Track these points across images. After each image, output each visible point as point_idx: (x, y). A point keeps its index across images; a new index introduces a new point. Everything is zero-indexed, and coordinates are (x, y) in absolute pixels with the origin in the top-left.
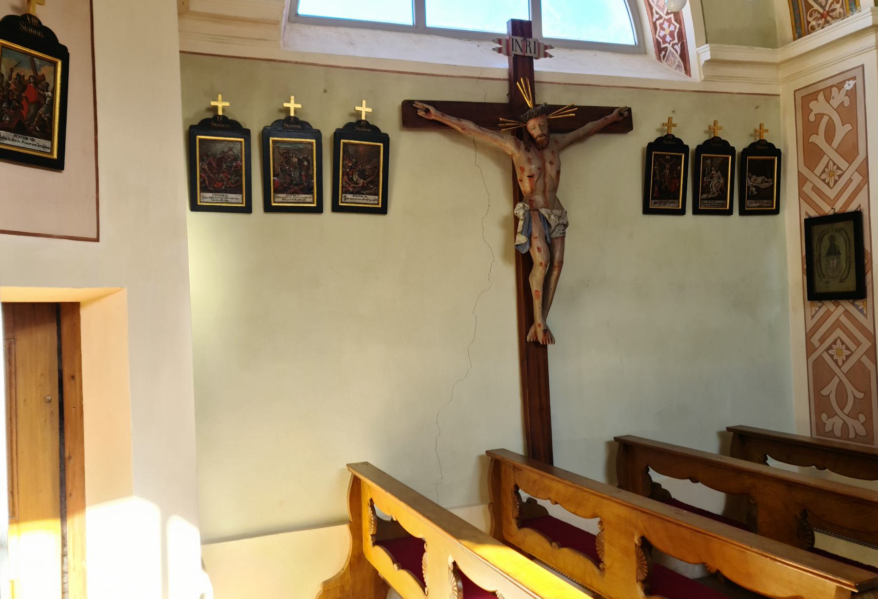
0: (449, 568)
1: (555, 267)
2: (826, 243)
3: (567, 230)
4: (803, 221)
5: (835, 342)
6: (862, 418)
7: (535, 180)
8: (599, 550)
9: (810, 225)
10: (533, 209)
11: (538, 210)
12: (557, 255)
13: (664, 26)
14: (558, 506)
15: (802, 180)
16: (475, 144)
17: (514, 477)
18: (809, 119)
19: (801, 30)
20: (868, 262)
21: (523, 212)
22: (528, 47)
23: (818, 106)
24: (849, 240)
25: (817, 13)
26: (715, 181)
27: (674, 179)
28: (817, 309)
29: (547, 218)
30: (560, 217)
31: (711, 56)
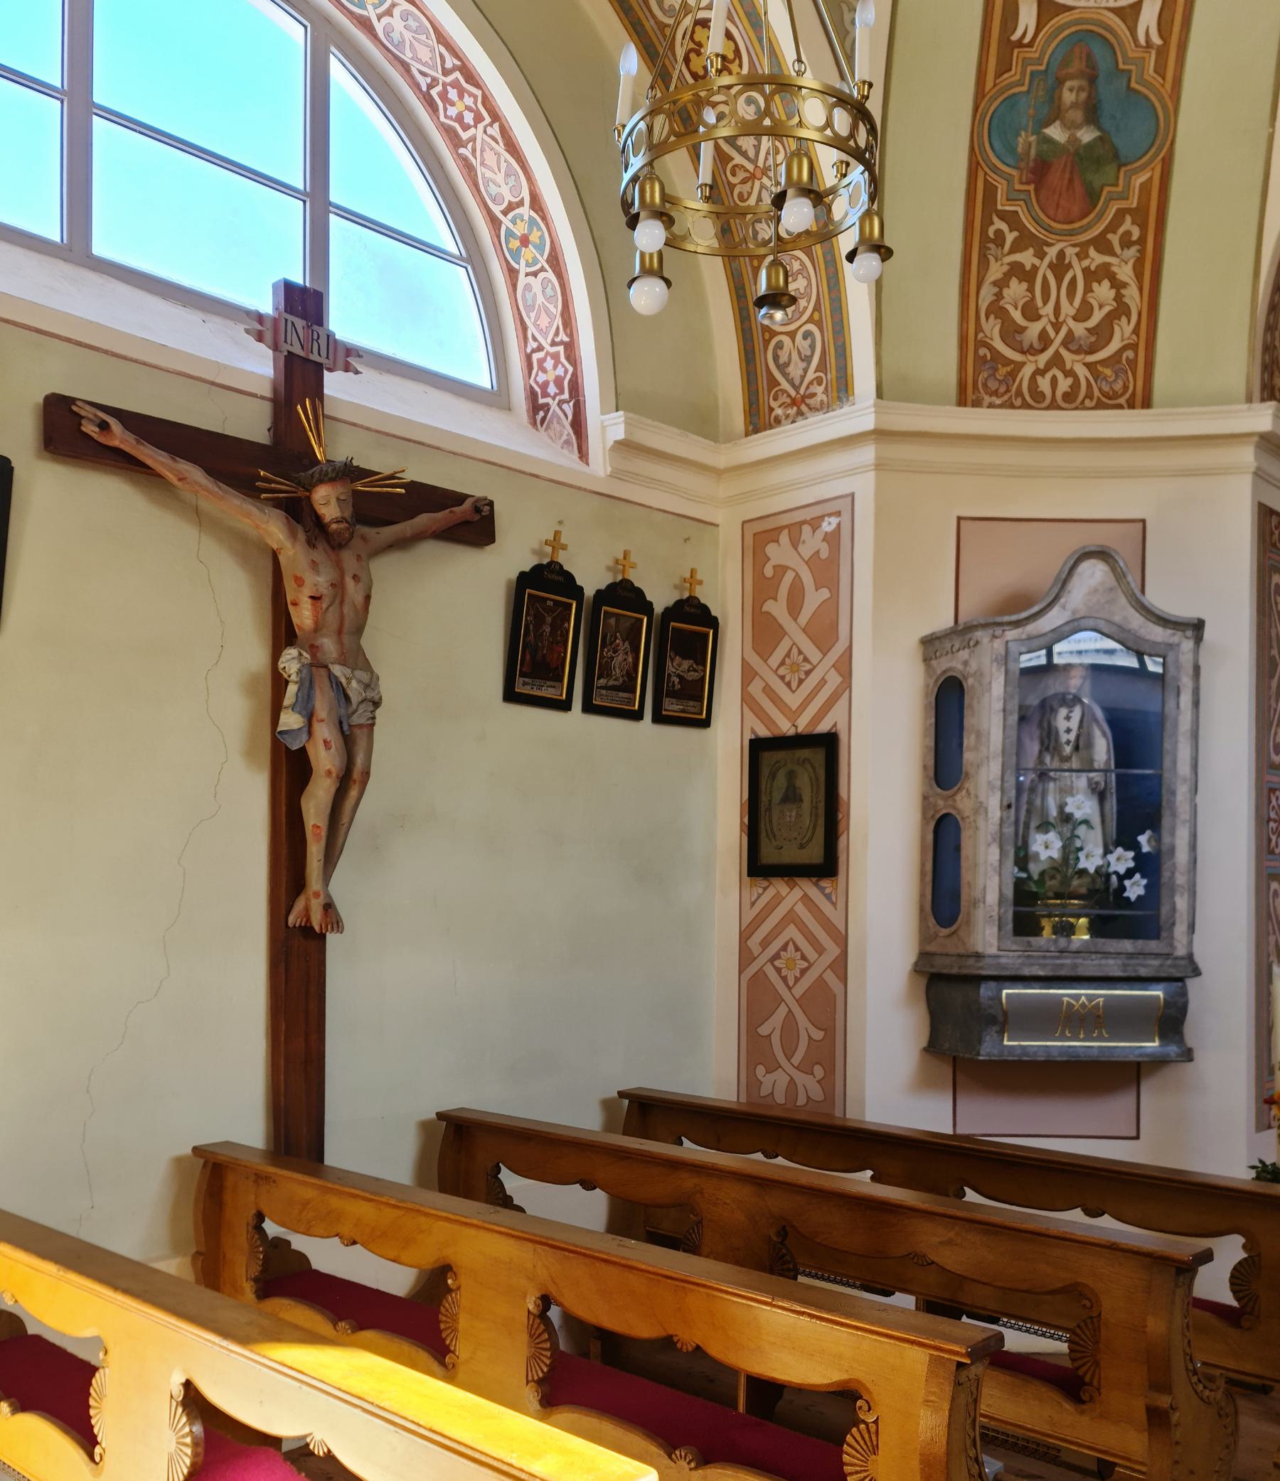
0: (172, 1397)
1: (355, 781)
2: (781, 780)
3: (378, 712)
4: (747, 744)
5: (784, 948)
6: (819, 1072)
7: (324, 606)
8: (446, 1329)
9: (758, 749)
10: (317, 664)
11: (326, 667)
12: (359, 760)
13: (545, 365)
14: (358, 1246)
15: (748, 674)
16: (198, 517)
17: (256, 1197)
18: (763, 573)
19: (758, 420)
20: (843, 817)
21: (298, 666)
22: (315, 342)
23: (778, 553)
24: (817, 779)
25: (785, 395)
26: (620, 658)
27: (557, 643)
28: (761, 891)
29: (345, 685)
30: (367, 686)
31: (625, 432)
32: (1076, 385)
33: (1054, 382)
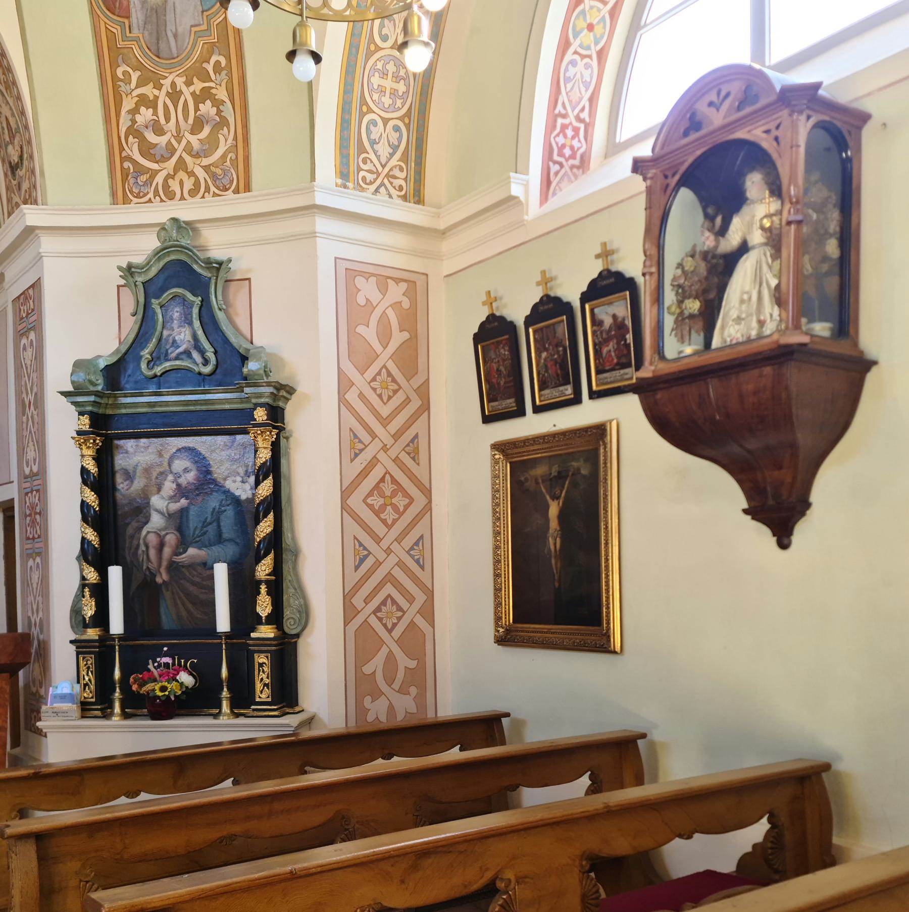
5: (384, 603)
32: (197, 184)
33: (181, 183)
